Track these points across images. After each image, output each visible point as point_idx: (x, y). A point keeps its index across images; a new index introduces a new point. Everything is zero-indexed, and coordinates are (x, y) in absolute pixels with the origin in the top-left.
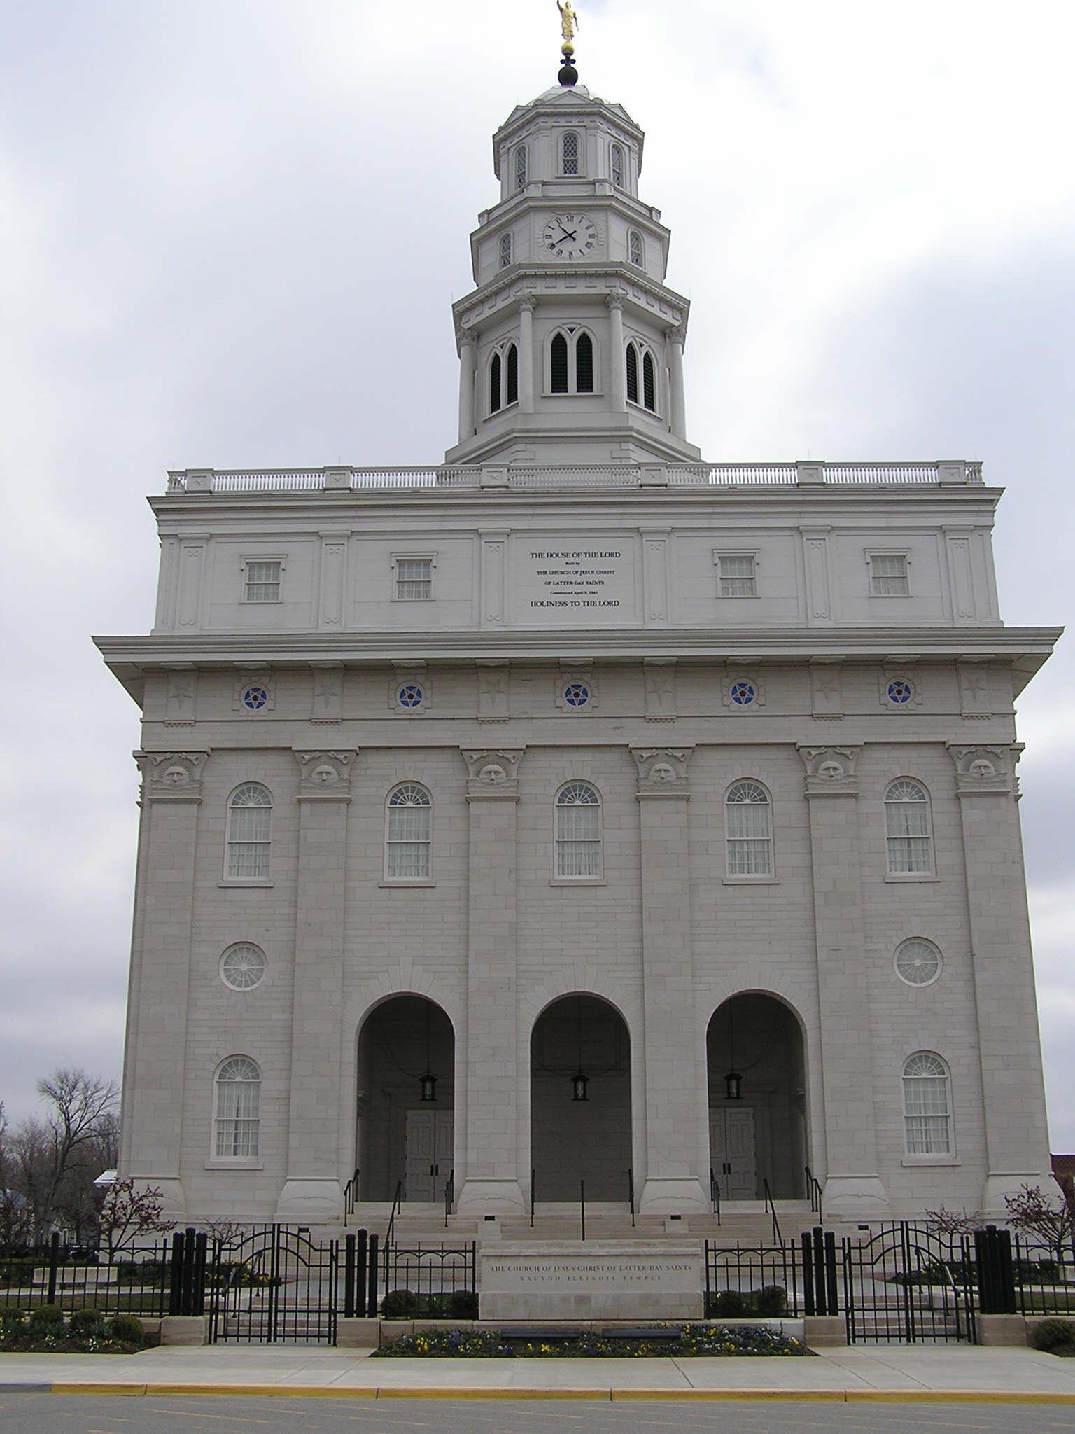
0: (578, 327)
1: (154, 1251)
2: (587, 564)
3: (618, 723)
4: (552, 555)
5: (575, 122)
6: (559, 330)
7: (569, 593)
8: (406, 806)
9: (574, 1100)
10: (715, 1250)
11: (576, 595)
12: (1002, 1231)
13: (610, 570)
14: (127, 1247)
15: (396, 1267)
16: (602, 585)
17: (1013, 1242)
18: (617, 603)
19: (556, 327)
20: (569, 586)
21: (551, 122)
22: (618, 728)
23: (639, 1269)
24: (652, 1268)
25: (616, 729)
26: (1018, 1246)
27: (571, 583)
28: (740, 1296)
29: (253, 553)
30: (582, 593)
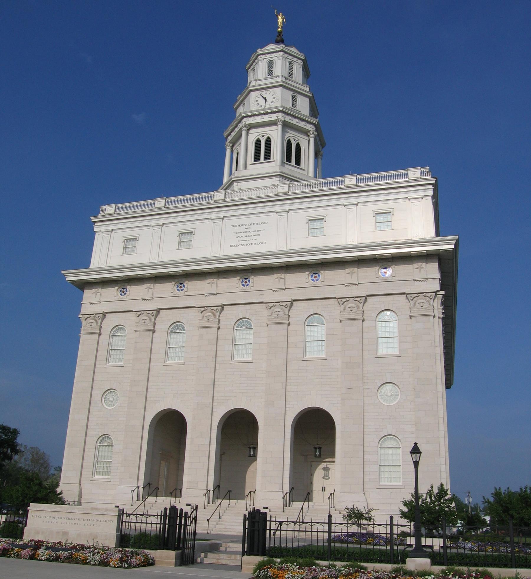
0: (265, 134)
1: (156, 517)
2: (253, 228)
3: (260, 293)
4: (240, 225)
5: (295, 59)
6: (258, 137)
7: (246, 240)
8: (177, 332)
9: (315, 457)
10: (397, 525)
11: (248, 241)
12: (263, 513)
13: (262, 229)
14: (135, 513)
15: (324, 532)
16: (259, 236)
17: (268, 519)
18: (265, 243)
19: (257, 136)
20: (246, 237)
21: (263, 57)
22: (261, 295)
23: (91, 521)
24: (97, 521)
25: (260, 296)
26: (271, 521)
27: (247, 236)
28: (130, 536)
29: (382, 253)
30: (251, 240)
